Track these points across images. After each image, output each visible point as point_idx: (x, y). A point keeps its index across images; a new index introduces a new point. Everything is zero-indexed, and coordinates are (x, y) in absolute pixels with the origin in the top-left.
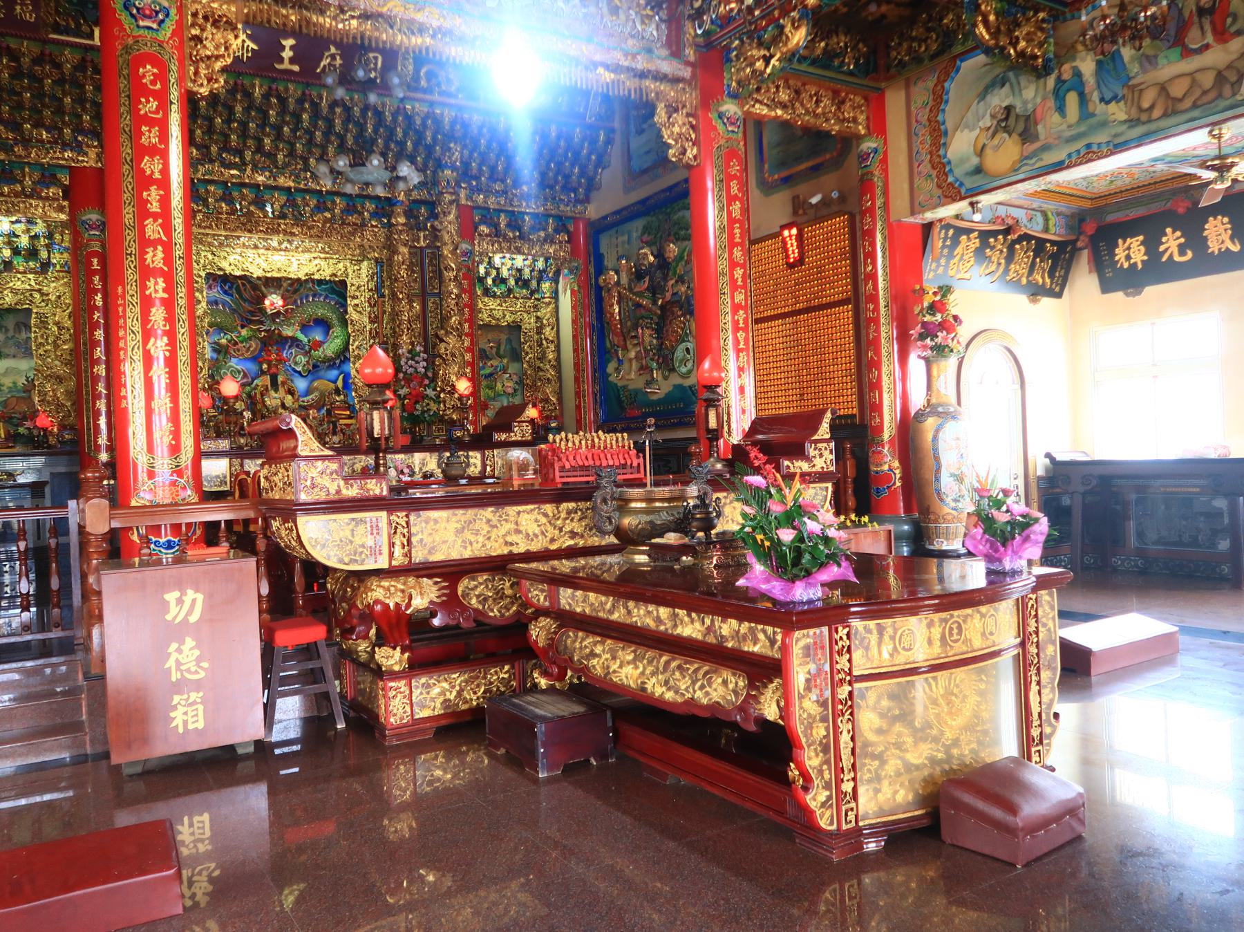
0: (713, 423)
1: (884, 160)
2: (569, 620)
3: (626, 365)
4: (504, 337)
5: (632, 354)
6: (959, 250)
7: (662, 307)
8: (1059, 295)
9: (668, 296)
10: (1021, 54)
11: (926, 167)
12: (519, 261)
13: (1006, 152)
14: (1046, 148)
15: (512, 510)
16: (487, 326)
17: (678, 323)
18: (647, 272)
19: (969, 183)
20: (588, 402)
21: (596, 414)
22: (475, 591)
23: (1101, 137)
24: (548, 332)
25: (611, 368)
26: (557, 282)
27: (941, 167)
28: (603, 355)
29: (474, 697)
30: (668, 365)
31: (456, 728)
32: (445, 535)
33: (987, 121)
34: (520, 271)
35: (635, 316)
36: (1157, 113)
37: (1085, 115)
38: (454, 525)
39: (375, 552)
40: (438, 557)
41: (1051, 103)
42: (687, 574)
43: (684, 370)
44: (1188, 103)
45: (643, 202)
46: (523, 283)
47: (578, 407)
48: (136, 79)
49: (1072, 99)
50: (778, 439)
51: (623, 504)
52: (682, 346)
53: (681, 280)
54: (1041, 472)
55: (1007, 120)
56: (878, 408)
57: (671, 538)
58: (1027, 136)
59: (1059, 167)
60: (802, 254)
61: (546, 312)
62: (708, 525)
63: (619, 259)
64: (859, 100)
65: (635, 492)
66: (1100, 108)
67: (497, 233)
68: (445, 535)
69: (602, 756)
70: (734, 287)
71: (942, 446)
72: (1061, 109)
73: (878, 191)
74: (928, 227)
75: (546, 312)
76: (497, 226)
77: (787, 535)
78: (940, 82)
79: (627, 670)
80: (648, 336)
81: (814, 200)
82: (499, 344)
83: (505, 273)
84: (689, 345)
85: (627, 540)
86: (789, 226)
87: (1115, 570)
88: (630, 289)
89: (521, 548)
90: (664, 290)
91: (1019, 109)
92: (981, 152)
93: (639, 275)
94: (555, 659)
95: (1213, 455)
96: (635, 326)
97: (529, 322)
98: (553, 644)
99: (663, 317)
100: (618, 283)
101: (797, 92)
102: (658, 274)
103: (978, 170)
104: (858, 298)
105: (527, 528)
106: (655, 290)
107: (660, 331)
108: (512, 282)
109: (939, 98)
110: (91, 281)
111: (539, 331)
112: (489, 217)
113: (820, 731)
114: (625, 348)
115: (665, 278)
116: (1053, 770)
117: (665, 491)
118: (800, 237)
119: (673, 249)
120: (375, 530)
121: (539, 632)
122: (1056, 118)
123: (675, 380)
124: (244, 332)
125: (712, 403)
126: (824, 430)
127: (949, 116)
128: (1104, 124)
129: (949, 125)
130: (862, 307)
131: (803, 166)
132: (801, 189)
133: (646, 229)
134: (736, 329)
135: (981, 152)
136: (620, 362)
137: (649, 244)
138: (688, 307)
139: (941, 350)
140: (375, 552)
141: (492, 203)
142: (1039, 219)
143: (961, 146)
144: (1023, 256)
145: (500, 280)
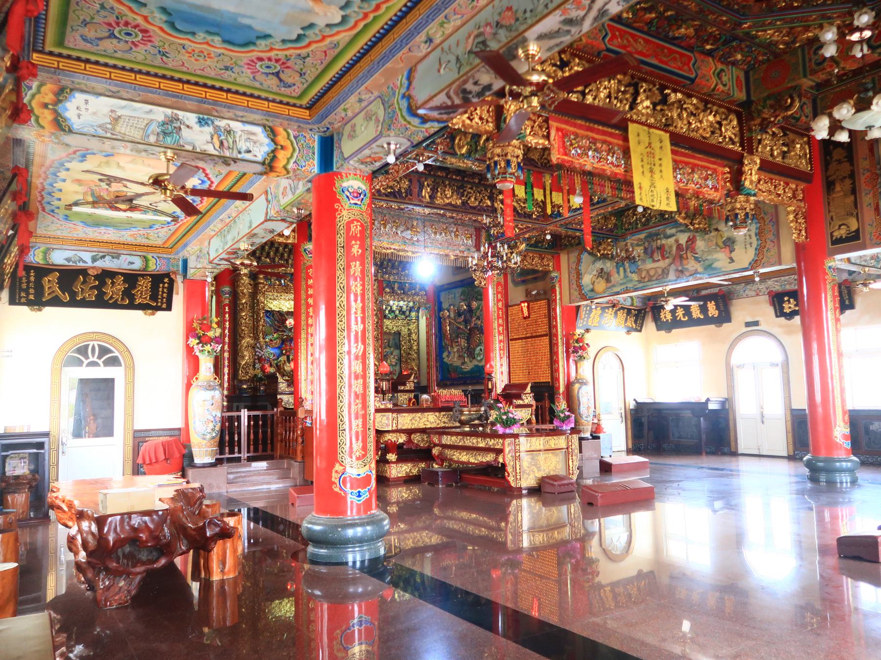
0: (490, 387)
1: (560, 281)
2: (445, 446)
3: (452, 354)
4: (391, 337)
5: (455, 350)
6: (592, 315)
7: (470, 330)
8: (640, 331)
9: (473, 325)
10: (603, 254)
11: (575, 286)
12: (401, 303)
13: (601, 285)
14: (614, 286)
15: (426, 414)
16: (386, 333)
17: (477, 337)
18: (463, 313)
19: (590, 294)
20: (434, 372)
21: (437, 377)
22: (416, 438)
23: (630, 285)
24: (414, 336)
25: (445, 355)
26: (418, 312)
27: (580, 286)
28: (441, 349)
29: (415, 471)
30: (472, 356)
31: (409, 480)
32: (407, 421)
33: (595, 273)
34: (401, 307)
35: (457, 333)
36: (646, 280)
37: (626, 277)
38: (410, 418)
39: (388, 425)
40: (404, 428)
41: (615, 270)
42: (480, 427)
43: (479, 358)
44: (654, 278)
45: (462, 281)
46: (402, 312)
47: (428, 373)
48: (307, 273)
49: (621, 269)
50: (511, 394)
51: (461, 412)
52: (479, 348)
53: (478, 318)
54: (632, 407)
55: (601, 273)
56: (558, 380)
57: (476, 422)
58: (608, 280)
59: (618, 293)
60: (529, 314)
61: (413, 327)
62: (487, 419)
63: (450, 305)
64: (550, 257)
65: (465, 409)
66: (630, 275)
67: (393, 291)
68: (407, 421)
69: (456, 483)
70: (499, 334)
71: (580, 395)
72: (618, 272)
73: (558, 293)
74: (579, 307)
75: (413, 327)
76: (393, 289)
77: (504, 417)
78: (579, 255)
79: (464, 457)
80: (463, 343)
81: (534, 293)
82: (389, 341)
83: (394, 308)
84: (482, 348)
85: (463, 423)
86: (524, 302)
87: (664, 450)
88: (455, 320)
89: (429, 426)
90: (470, 322)
91: (605, 270)
92: (593, 284)
93: (459, 314)
94: (442, 459)
95: (693, 401)
96: (457, 337)
97: (404, 331)
98: (441, 453)
99: (470, 334)
100: (449, 316)
101: (525, 256)
102: (468, 314)
103: (592, 290)
104: (551, 335)
105: (431, 420)
106: (466, 322)
107: (468, 340)
108: (397, 312)
109: (579, 261)
110: (224, 317)
111: (410, 335)
112: (390, 285)
113: (512, 463)
114: (452, 346)
115: (471, 317)
116: (245, 174)
117: (473, 409)
118: (528, 307)
119: (475, 304)
120: (388, 419)
121: (435, 451)
122: (617, 275)
123: (475, 363)
124: (275, 335)
125: (490, 379)
126: (528, 390)
127: (583, 268)
128: (631, 281)
129: (583, 271)
130: (552, 336)
131: (530, 277)
132: (530, 286)
133: (462, 293)
134: (500, 349)
135: (593, 284)
136: (449, 353)
137: (464, 300)
138: (481, 330)
139: (582, 358)
140: (388, 425)
141: (392, 278)
142: (629, 300)
143: (587, 280)
144: (622, 315)
145: (391, 311)
